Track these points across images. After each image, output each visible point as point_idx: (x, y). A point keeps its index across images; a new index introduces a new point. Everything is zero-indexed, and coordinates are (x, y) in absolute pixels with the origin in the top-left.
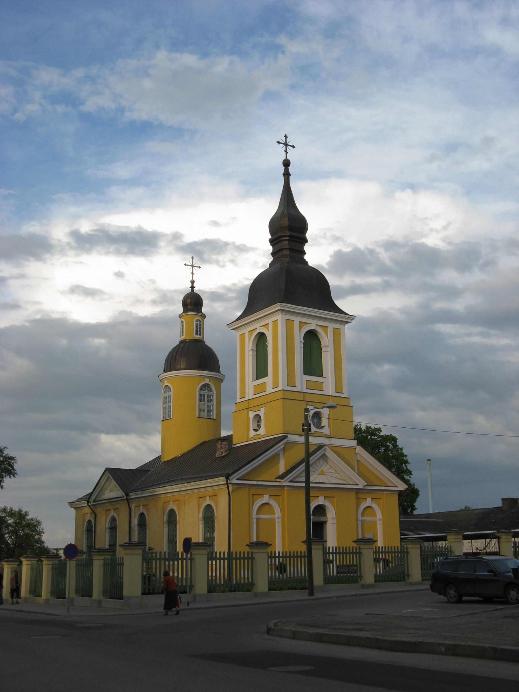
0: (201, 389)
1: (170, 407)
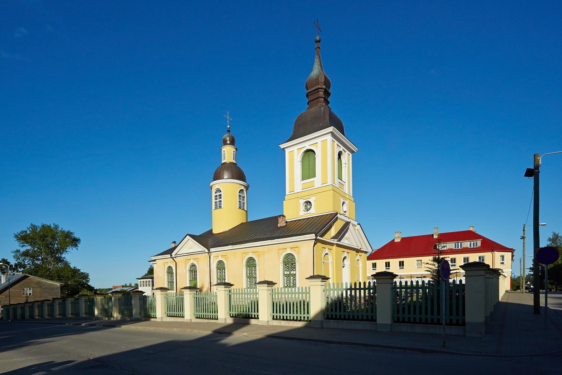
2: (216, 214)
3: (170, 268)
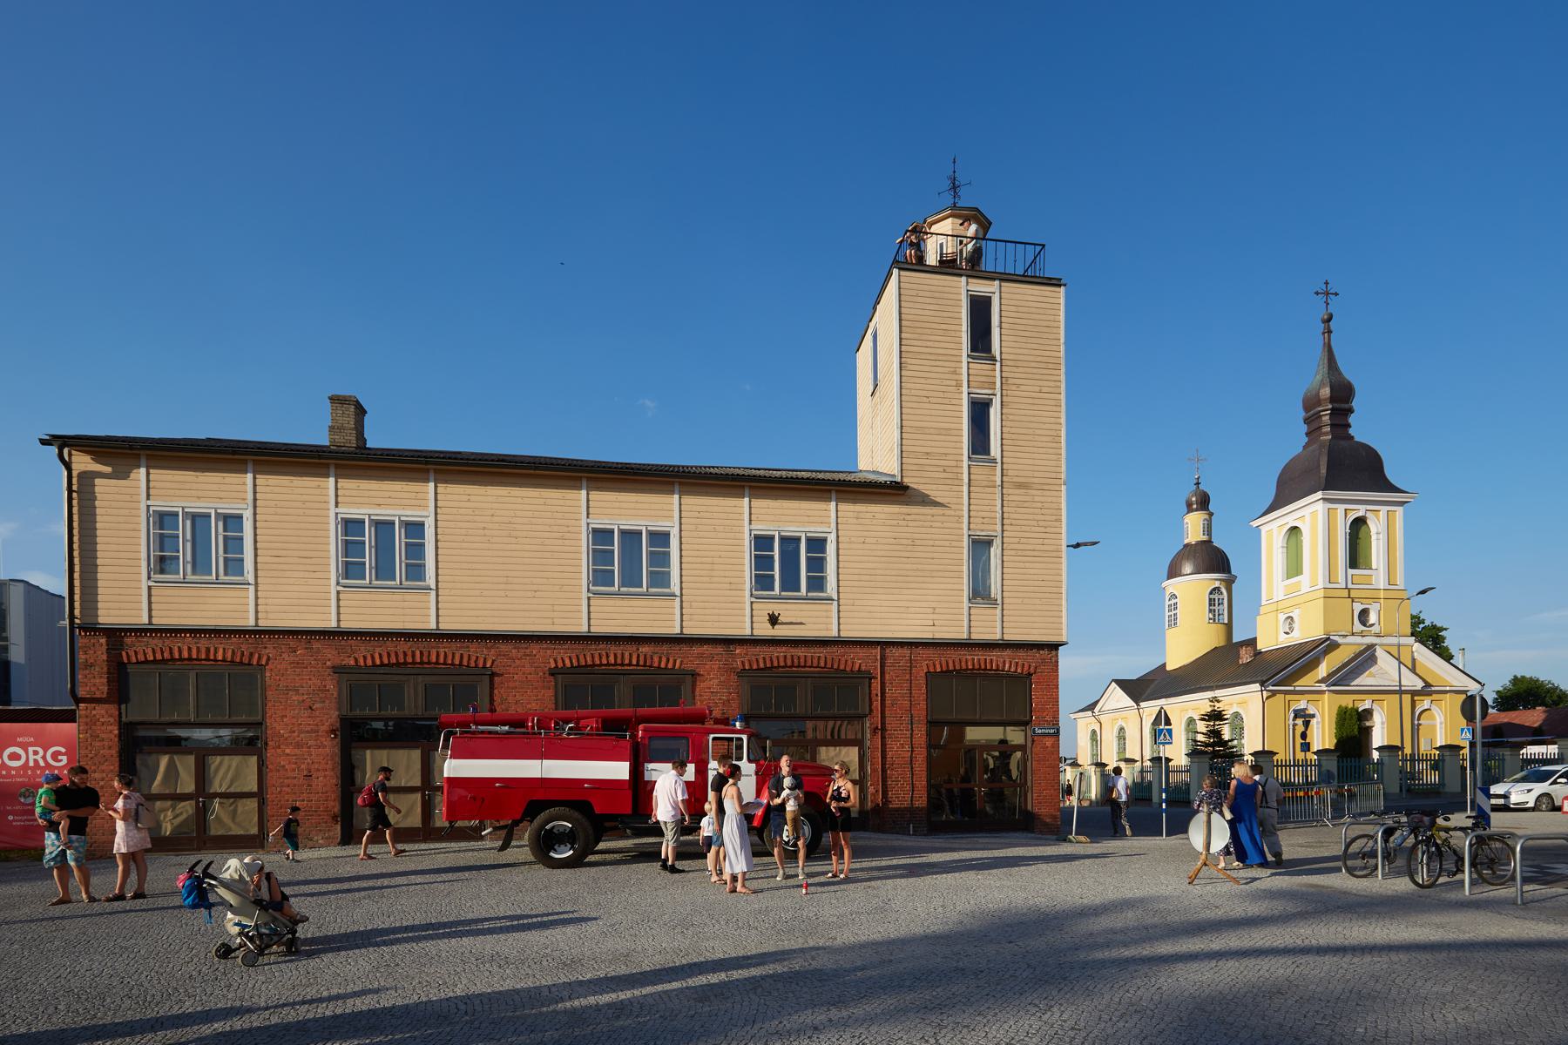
2: (1171, 635)
3: (1094, 732)
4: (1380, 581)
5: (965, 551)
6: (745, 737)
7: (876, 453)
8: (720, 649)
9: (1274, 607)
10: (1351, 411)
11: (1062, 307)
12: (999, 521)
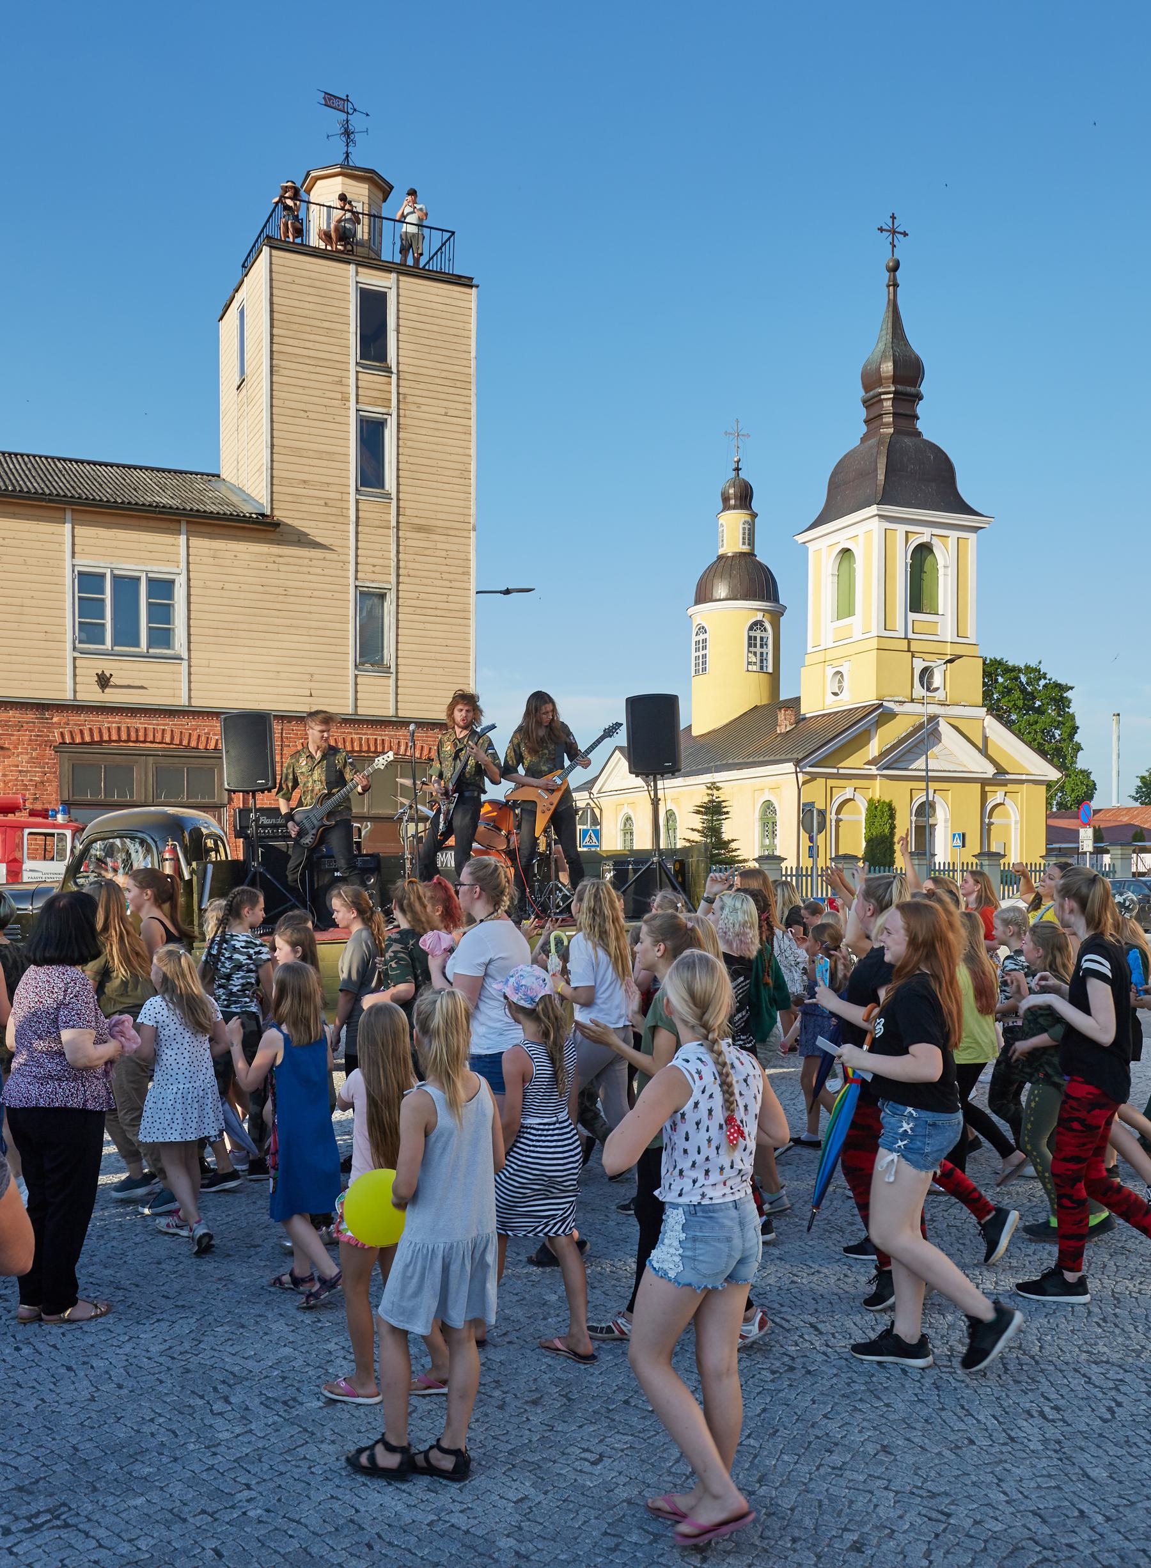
0: (751, 628)
1: (697, 650)
4: (946, 629)
5: (352, 605)
6: (68, 833)
7: (244, 469)
8: (30, 716)
9: (820, 657)
10: (919, 397)
11: (474, 313)
12: (393, 571)
